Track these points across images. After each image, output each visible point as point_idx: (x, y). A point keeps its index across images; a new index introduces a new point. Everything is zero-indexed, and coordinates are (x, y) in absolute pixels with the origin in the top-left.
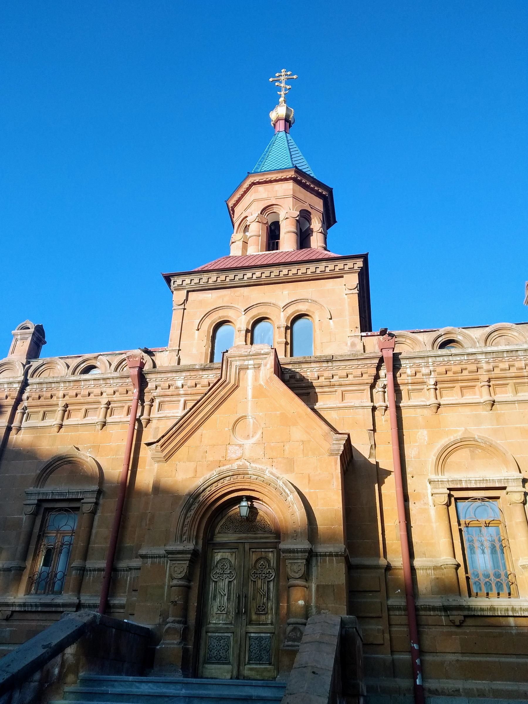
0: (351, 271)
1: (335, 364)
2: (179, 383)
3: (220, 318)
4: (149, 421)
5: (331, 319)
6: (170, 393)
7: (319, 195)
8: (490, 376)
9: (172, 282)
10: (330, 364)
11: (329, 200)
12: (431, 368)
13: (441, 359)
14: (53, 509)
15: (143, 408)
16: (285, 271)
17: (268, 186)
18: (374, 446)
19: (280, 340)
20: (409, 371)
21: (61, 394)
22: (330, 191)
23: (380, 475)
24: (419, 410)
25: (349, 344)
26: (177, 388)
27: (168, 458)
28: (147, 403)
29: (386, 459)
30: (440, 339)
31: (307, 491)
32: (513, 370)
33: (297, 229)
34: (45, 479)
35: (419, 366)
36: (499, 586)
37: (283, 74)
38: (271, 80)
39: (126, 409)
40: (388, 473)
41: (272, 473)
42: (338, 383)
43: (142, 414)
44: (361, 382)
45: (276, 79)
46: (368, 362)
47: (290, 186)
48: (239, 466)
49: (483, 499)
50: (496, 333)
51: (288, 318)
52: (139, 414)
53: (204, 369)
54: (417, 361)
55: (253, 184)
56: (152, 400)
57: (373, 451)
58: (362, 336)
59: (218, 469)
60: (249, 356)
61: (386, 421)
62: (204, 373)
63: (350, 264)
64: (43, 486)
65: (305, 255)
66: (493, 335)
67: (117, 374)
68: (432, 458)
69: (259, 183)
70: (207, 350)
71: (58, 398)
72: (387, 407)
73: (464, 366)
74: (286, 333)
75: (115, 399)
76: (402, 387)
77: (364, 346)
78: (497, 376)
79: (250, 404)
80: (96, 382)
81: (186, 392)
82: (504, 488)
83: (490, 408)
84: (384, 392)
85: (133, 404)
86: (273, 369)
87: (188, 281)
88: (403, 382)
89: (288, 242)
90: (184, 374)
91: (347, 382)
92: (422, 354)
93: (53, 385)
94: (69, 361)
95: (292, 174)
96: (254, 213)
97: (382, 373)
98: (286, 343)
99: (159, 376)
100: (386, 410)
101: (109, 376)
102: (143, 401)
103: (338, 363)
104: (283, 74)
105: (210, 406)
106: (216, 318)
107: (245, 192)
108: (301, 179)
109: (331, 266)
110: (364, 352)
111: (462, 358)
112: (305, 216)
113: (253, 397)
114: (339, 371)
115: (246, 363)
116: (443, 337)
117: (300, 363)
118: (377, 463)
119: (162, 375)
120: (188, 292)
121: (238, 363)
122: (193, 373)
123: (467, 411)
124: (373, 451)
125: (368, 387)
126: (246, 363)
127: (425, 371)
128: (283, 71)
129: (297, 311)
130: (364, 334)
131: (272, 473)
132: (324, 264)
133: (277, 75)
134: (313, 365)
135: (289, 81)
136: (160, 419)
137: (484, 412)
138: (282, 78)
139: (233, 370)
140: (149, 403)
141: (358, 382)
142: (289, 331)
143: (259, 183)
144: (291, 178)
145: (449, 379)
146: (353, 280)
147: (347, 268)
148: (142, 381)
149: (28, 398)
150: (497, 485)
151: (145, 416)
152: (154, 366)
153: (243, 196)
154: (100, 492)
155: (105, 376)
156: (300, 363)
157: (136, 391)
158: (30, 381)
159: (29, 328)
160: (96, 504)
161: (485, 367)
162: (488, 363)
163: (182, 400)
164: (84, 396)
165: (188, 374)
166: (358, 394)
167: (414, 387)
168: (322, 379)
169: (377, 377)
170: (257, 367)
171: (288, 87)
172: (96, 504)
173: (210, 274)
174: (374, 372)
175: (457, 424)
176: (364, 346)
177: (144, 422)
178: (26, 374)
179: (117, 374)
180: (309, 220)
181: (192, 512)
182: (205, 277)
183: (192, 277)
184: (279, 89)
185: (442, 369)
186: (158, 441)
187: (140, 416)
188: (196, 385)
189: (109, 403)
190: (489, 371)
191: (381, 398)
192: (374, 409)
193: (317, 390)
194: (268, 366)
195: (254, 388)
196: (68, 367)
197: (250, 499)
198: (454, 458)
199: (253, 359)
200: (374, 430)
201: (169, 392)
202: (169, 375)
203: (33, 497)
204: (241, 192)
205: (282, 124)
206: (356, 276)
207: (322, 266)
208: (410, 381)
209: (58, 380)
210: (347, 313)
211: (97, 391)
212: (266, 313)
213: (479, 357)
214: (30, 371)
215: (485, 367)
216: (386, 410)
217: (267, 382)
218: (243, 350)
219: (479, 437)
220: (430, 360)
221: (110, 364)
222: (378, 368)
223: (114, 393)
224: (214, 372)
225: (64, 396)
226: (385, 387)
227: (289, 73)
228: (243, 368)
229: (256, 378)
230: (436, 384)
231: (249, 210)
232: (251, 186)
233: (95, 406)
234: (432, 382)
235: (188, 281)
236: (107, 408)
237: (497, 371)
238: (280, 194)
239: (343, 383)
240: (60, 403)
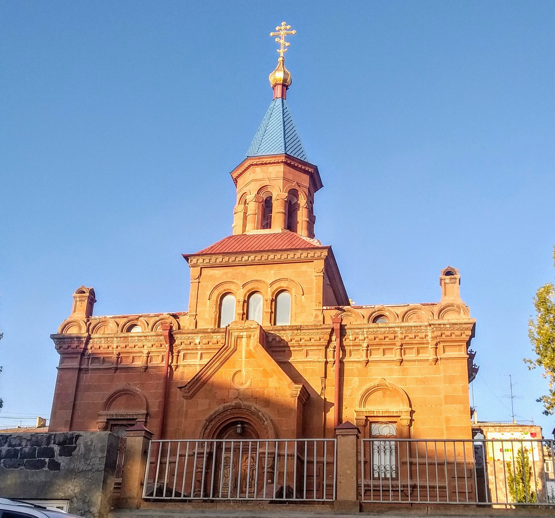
0: (319, 258)
2: (197, 341)
3: (225, 290)
5: (303, 295)
6: (190, 348)
8: (403, 342)
9: (189, 260)
12: (365, 336)
13: (372, 330)
14: (116, 425)
16: (272, 256)
17: (264, 168)
18: (324, 388)
19: (267, 310)
20: (351, 338)
21: (115, 346)
22: (316, 168)
23: (326, 406)
24: (355, 364)
25: (314, 316)
26: (196, 344)
27: (191, 397)
29: (331, 396)
30: (374, 314)
32: (417, 339)
34: (110, 405)
35: (358, 334)
36: (118, 472)
37: (283, 30)
38: (271, 34)
39: (160, 358)
40: (333, 404)
41: (255, 408)
42: (304, 344)
43: (172, 362)
44: (319, 344)
46: (324, 331)
47: (281, 168)
48: (236, 403)
49: (386, 423)
50: (411, 311)
51: (274, 292)
52: (170, 361)
54: (357, 331)
55: (252, 165)
56: (179, 352)
58: (323, 310)
59: (223, 405)
60: (242, 330)
61: (333, 371)
62: (214, 334)
63: (318, 253)
66: (409, 312)
67: (153, 333)
70: (216, 315)
71: (113, 348)
72: (335, 362)
73: (386, 335)
74: (271, 305)
75: (153, 350)
77: (324, 317)
78: (407, 342)
79: (243, 362)
81: (202, 347)
83: (399, 364)
84: (334, 351)
85: (166, 354)
86: (258, 340)
87: (201, 260)
88: (347, 344)
90: (200, 335)
91: (310, 344)
92: (360, 326)
93: (109, 339)
95: (283, 159)
96: (253, 189)
97: (334, 338)
98: (271, 313)
99: (183, 336)
100: (334, 364)
101: (148, 334)
102: (172, 353)
103: (305, 331)
104: (283, 28)
105: (218, 363)
106: (221, 290)
107: (245, 170)
109: (305, 254)
110: (324, 323)
111: (386, 330)
112: (293, 193)
114: (305, 336)
115: (241, 334)
116: (377, 313)
117: (279, 330)
119: (185, 335)
120: (201, 268)
121: (236, 334)
122: (206, 335)
123: (385, 365)
125: (324, 348)
126: (241, 334)
127: (361, 337)
128: (282, 24)
129: (280, 287)
130: (325, 308)
131: (255, 408)
134: (288, 332)
135: (288, 38)
136: (184, 366)
137: (396, 367)
139: (233, 339)
140: (177, 354)
141: (317, 344)
142: (274, 303)
144: (282, 162)
145: (376, 343)
146: (321, 265)
147: (316, 255)
148: (171, 339)
149: (91, 348)
150: (395, 415)
152: (179, 328)
153: (243, 172)
154: (147, 415)
155: (145, 334)
156: (279, 330)
159: (84, 293)
162: (402, 333)
163: (200, 352)
165: (203, 335)
166: (318, 352)
167: (354, 348)
168: (293, 341)
169: (330, 341)
170: (249, 337)
171: (287, 44)
175: (379, 374)
176: (324, 317)
177: (174, 368)
179: (153, 333)
180: (297, 196)
181: (208, 430)
182: (214, 258)
184: (278, 45)
185: (372, 337)
186: (185, 386)
187: (171, 363)
188: (208, 343)
189: (149, 353)
190: (402, 339)
191: (332, 355)
192: (326, 363)
193: (291, 349)
194: (256, 337)
195: (246, 351)
196: (118, 325)
197: (242, 423)
198: (372, 397)
199: (247, 331)
200: (326, 377)
201: (190, 347)
202: (190, 335)
203: (104, 417)
204: (242, 169)
205: (279, 89)
207: (298, 254)
208: (351, 344)
211: (140, 344)
213: (396, 329)
214: (91, 328)
216: (334, 364)
217: (254, 349)
219: (389, 384)
221: (148, 325)
222: (331, 335)
223: (152, 346)
224: (220, 334)
225: (117, 347)
226: (335, 347)
227: (288, 27)
228: (239, 337)
229: (248, 345)
230: (368, 346)
231: (248, 188)
232: (250, 166)
234: (365, 345)
236: (148, 357)
237: (407, 339)
238: (273, 176)
239: (307, 344)
240: (114, 352)
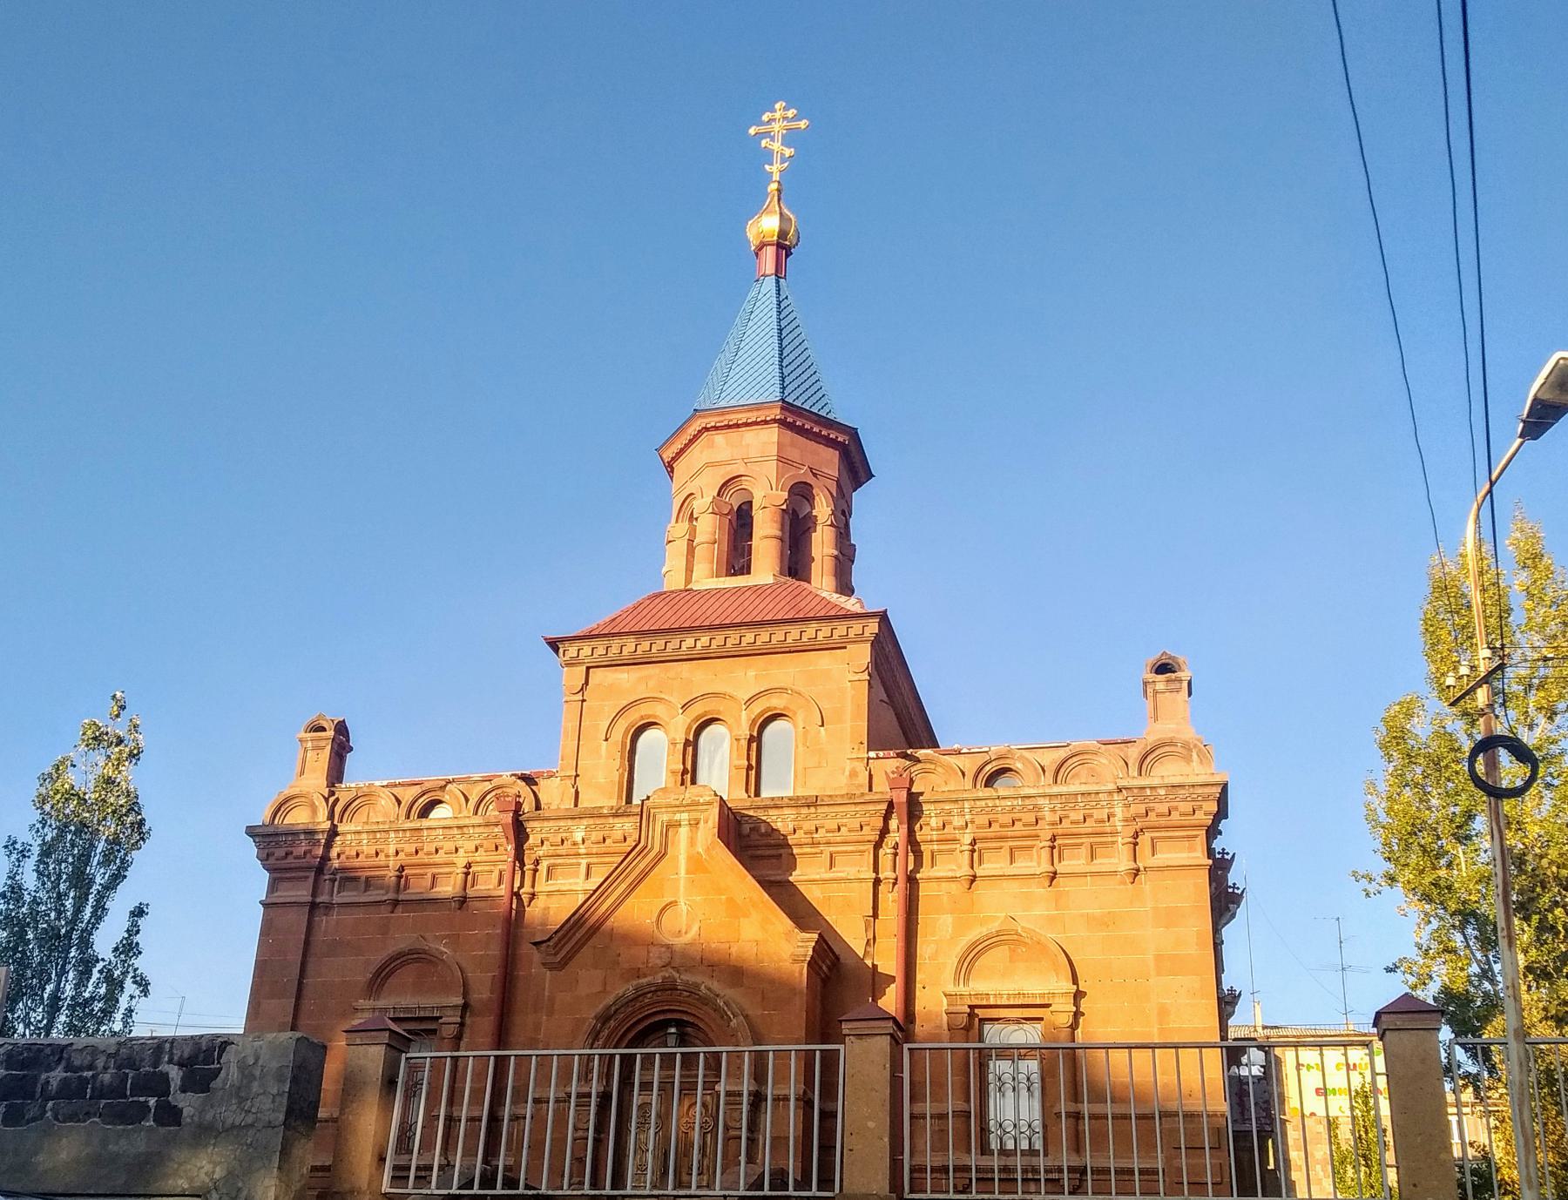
0: (859, 639)
1: (820, 810)
2: (578, 836)
3: (642, 718)
4: (533, 896)
7: (831, 443)
10: (812, 810)
11: (853, 448)
13: (983, 803)
15: (523, 873)
17: (733, 435)
20: (934, 822)
21: (392, 851)
22: (853, 433)
28: (528, 866)
29: (888, 961)
30: (988, 768)
31: (759, 1012)
33: (782, 530)
34: (382, 985)
35: (950, 813)
38: (752, 131)
40: (892, 979)
45: (762, 129)
46: (871, 807)
47: (772, 434)
49: (1018, 1021)
52: (517, 884)
53: (615, 815)
55: (706, 429)
56: (537, 862)
57: (870, 949)
60: (680, 807)
61: (892, 901)
64: (377, 998)
65: (787, 608)
67: (477, 820)
68: (952, 962)
69: (716, 428)
70: (621, 776)
73: (1017, 816)
76: (923, 848)
80: (447, 832)
82: (1048, 1006)
85: (507, 867)
87: (586, 651)
89: (765, 566)
90: (585, 822)
92: (954, 796)
94: (398, 791)
95: (776, 413)
97: (893, 824)
98: (749, 768)
99: (546, 824)
101: (467, 822)
102: (522, 865)
103: (825, 809)
104: (778, 115)
105: (624, 886)
106: (634, 717)
108: (798, 420)
109: (825, 631)
112: (801, 493)
113: (688, 872)
114: (827, 819)
115: (677, 817)
117: (766, 807)
118: (875, 966)
119: (551, 823)
120: (588, 668)
121: (665, 818)
123: (1013, 887)
124: (870, 949)
125: (871, 847)
127: (958, 821)
128: (777, 106)
129: (769, 709)
130: (872, 754)
132: (815, 625)
133: (765, 118)
134: (786, 811)
136: (550, 894)
137: (1039, 890)
138: (776, 127)
143: (716, 428)
144: (775, 421)
148: (519, 833)
150: (1038, 1002)
151: (527, 888)
152: (538, 807)
154: (465, 1007)
155: (461, 823)
156: (766, 807)
157: (510, 848)
158: (340, 829)
159: (324, 729)
160: (462, 1025)
161: (1049, 816)
163: (584, 862)
164: (428, 854)
165: (591, 821)
166: (857, 857)
168: (800, 833)
169: (884, 831)
170: (694, 824)
172: (462, 1025)
173: (625, 640)
174: (880, 824)
175: (1000, 905)
177: (525, 898)
178: (331, 816)
179: (477, 820)
182: (615, 644)
183: (594, 643)
185: (983, 820)
189: (469, 866)
192: (877, 882)
194: (710, 824)
195: (690, 858)
196: (399, 802)
200: (875, 916)
201: (562, 850)
202: (562, 823)
204: (684, 439)
205: (770, 252)
206: (866, 649)
209: (386, 827)
210: (848, 716)
211: (449, 846)
212: (719, 712)
213: (1041, 801)
214: (338, 809)
215: (1049, 816)
217: (708, 850)
218: (673, 796)
220: (967, 805)
222: (887, 818)
224: (632, 819)
227: (791, 113)
228: (672, 825)
229: (692, 842)
233: (447, 870)
234: (967, 839)
235: (586, 651)
237: (1066, 823)
